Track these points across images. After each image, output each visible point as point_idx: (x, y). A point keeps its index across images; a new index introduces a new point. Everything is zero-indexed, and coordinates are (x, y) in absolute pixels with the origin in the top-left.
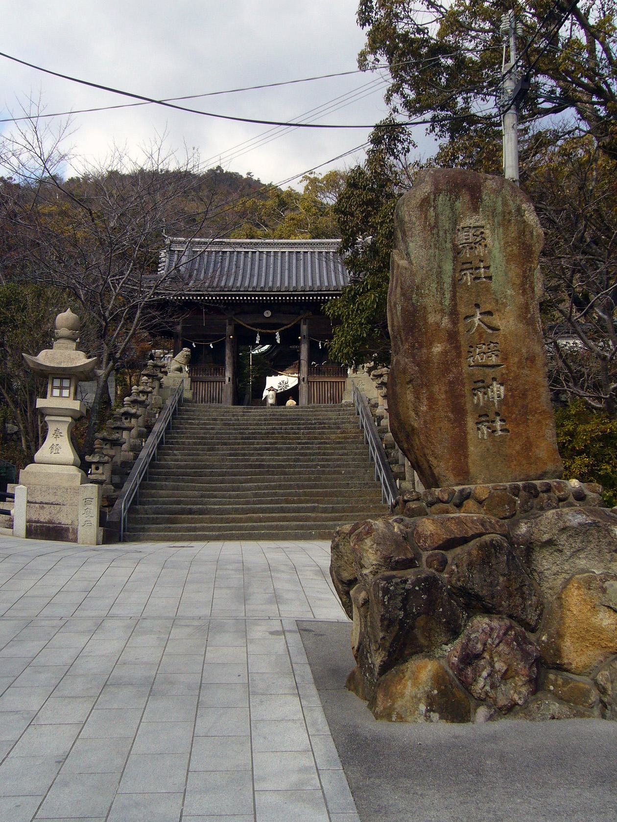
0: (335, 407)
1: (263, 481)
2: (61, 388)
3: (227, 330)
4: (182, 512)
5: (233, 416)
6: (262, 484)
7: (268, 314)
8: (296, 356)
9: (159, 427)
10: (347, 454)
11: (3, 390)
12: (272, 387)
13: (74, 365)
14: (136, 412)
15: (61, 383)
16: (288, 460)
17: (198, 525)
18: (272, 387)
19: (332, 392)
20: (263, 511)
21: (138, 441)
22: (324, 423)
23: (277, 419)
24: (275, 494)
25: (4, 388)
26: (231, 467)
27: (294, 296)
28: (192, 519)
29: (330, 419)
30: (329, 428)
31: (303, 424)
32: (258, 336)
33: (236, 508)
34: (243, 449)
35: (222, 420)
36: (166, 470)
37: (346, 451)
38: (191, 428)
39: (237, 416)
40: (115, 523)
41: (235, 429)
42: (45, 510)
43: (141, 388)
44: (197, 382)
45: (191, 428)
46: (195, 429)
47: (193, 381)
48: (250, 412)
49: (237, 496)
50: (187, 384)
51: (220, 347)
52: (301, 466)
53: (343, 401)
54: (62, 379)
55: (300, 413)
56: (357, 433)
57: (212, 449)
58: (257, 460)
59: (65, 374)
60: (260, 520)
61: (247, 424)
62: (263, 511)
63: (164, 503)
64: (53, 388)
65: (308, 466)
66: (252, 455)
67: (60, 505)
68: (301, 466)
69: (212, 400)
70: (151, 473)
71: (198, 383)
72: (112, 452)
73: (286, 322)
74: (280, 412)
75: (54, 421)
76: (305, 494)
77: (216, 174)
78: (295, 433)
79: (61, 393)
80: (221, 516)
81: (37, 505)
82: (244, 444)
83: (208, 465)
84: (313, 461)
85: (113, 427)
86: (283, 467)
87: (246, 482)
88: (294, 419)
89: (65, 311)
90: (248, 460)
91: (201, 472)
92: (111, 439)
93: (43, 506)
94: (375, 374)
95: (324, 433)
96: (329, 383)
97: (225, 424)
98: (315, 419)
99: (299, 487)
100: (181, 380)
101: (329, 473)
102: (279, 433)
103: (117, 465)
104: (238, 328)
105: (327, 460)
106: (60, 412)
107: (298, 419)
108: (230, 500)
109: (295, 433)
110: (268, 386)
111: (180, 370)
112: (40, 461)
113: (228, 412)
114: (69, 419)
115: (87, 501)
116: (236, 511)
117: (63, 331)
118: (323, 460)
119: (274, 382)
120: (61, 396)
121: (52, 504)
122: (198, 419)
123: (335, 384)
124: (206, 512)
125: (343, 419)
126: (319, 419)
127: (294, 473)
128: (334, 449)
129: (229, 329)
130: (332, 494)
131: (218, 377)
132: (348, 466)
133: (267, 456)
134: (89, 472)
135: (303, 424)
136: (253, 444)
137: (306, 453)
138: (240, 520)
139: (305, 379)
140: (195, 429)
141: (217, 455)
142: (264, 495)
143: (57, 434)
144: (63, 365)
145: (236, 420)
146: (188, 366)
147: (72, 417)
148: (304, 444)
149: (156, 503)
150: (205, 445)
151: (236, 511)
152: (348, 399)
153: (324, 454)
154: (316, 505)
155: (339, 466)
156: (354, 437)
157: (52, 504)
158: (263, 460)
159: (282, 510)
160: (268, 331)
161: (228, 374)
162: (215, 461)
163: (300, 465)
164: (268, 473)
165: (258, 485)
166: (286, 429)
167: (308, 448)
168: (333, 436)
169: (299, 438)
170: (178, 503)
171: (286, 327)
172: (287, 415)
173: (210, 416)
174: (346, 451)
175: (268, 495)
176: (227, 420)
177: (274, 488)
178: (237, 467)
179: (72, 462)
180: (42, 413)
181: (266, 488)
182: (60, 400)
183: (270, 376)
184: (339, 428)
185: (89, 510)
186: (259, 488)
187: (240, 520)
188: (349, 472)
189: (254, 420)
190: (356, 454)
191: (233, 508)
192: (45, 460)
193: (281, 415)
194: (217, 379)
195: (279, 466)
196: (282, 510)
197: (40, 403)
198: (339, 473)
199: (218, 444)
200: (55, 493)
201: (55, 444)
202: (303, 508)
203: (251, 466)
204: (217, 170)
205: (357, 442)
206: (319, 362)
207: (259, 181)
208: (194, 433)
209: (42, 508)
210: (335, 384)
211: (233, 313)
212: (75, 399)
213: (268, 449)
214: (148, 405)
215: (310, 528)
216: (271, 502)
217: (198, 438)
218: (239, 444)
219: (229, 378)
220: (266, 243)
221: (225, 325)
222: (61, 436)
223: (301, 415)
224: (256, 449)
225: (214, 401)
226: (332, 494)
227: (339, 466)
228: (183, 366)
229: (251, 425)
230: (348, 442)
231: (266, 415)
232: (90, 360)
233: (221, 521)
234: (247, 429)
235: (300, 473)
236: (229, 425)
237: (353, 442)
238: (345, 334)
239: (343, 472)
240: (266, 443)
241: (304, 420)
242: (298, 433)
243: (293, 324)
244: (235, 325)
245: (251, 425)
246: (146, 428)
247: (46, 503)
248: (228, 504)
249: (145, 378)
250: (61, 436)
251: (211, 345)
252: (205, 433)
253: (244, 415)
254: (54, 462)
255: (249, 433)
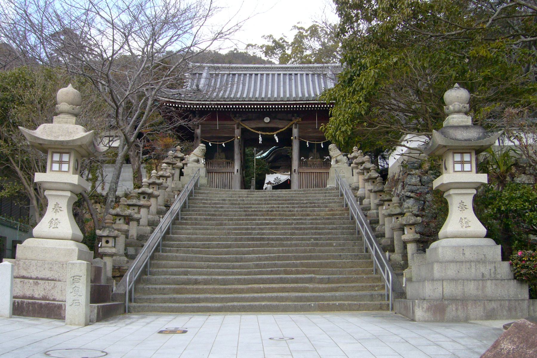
0: (321, 190)
1: (264, 252)
2: (61, 162)
3: (236, 133)
4: (188, 282)
5: (240, 197)
6: (263, 255)
7: (267, 120)
8: (289, 159)
9: (176, 206)
10: (336, 229)
11: (17, 168)
12: (270, 182)
13: (71, 139)
14: (153, 192)
15: (61, 157)
16: (285, 234)
17: (202, 296)
18: (270, 182)
19: (317, 180)
20: (264, 281)
21: (157, 218)
22: (314, 203)
23: (275, 200)
24: (275, 265)
25: (18, 167)
26: (236, 240)
27: (287, 104)
28: (197, 289)
29: (319, 200)
30: (319, 207)
31: (297, 204)
32: (260, 136)
33: (238, 279)
34: (247, 224)
35: (230, 200)
36: (178, 243)
37: (335, 226)
38: (204, 207)
39: (242, 197)
40: (121, 294)
41: (240, 208)
42: (39, 286)
43: (161, 173)
44: (213, 172)
45: (204, 207)
46: (207, 207)
47: (208, 172)
48: (253, 194)
49: (240, 267)
50: (203, 172)
51: (230, 147)
52: (297, 239)
53: (328, 186)
54: (61, 153)
55: (293, 195)
56: (343, 211)
57: (221, 224)
58: (258, 234)
59: (64, 149)
60: (261, 291)
61: (250, 204)
62: (264, 281)
63: (173, 274)
64: (52, 162)
65: (302, 239)
66: (254, 229)
67: (55, 280)
68: (297, 239)
69: (224, 186)
70: (164, 246)
71: (214, 173)
72: (125, 227)
73: (280, 126)
74: (277, 194)
75: (61, 196)
76: (302, 265)
77: (234, 53)
78: (290, 211)
79: (60, 168)
80: (224, 287)
81: (31, 281)
82: (247, 219)
83: (216, 238)
84: (307, 234)
85: (125, 203)
86: (281, 240)
87: (248, 253)
88: (289, 200)
89: (66, 87)
90: (250, 234)
91: (209, 244)
92: (123, 214)
93: (37, 282)
94: (357, 162)
95: (314, 211)
96: (315, 174)
97: (232, 204)
98: (306, 200)
99: (296, 258)
100: (197, 169)
101: (322, 245)
102: (277, 211)
103: (134, 239)
104: (244, 131)
105: (319, 234)
106: (58, 187)
107: (293, 200)
108: (233, 270)
109: (290, 211)
110: (266, 181)
111: (198, 161)
112: (39, 236)
113: (235, 194)
114: (69, 194)
115: (75, 279)
116: (239, 282)
117: (63, 106)
118: (315, 234)
119: (270, 178)
120: (60, 170)
121: (48, 279)
122: (210, 200)
123: (319, 174)
124: (211, 282)
125: (329, 199)
126: (309, 200)
127: (291, 246)
128: (324, 224)
129: (237, 132)
130: (327, 265)
131: (229, 169)
132: (339, 239)
133: (267, 230)
134: (99, 246)
135: (297, 204)
136: (255, 220)
137: (301, 227)
138: (242, 291)
139: (296, 171)
140: (207, 207)
141: (224, 229)
142: (264, 266)
143: (57, 208)
144: (61, 139)
145: (241, 200)
146: (203, 158)
147: (71, 192)
148: (298, 219)
149: (165, 273)
150: (214, 221)
151: (239, 282)
152: (331, 184)
153: (316, 228)
154: (313, 275)
155: (330, 239)
156: (340, 215)
157: (48, 279)
158: (263, 234)
159: (282, 281)
160: (267, 133)
161: (237, 166)
162: (221, 235)
163: (296, 238)
164: (267, 245)
165: (259, 257)
166: (282, 207)
167: (302, 223)
168: (323, 213)
169: (294, 215)
170: (186, 273)
171: (281, 130)
172: (283, 197)
173: (220, 197)
174: (335, 226)
175: (268, 266)
176: (234, 200)
177: (273, 259)
178: (241, 240)
179: (70, 236)
180: (38, 188)
181: (267, 259)
182: (59, 174)
183: (268, 174)
184: (326, 207)
185: (77, 289)
186: (260, 259)
187: (242, 291)
188: (340, 245)
189: (256, 200)
190: (343, 228)
191: (235, 279)
192: (44, 234)
193: (278, 197)
194: (228, 171)
195: (277, 239)
196: (282, 281)
197: (39, 177)
198: (331, 245)
199: (225, 219)
200: (51, 268)
201: (54, 219)
202: (301, 278)
203: (253, 239)
204: (234, 51)
205: (343, 218)
206: (307, 157)
207: (261, 58)
208: (206, 211)
209: (37, 284)
210: (319, 174)
211: (240, 119)
212: (74, 173)
213: (268, 224)
214: (167, 188)
215: (308, 299)
216: (271, 273)
217: (209, 215)
218: (243, 220)
219: (237, 170)
220: (266, 68)
221: (234, 129)
222: (61, 210)
223: (295, 197)
224: (257, 224)
225: (226, 188)
226: (327, 265)
227: (330, 239)
228: (200, 158)
229: (253, 204)
230: (335, 219)
231: (266, 197)
232: (88, 133)
233: (225, 291)
234: (251, 207)
235: (296, 245)
236: (235, 204)
237: (340, 218)
238: (343, 113)
239: (334, 244)
240: (266, 219)
241: (297, 200)
242: (293, 211)
243: (286, 127)
244: (242, 129)
245: (253, 204)
246: (165, 206)
247: (42, 279)
248: (231, 275)
249: (165, 164)
250: (61, 210)
251: (223, 144)
252: (215, 211)
253: (248, 197)
254: (49, 237)
255: (252, 211)
